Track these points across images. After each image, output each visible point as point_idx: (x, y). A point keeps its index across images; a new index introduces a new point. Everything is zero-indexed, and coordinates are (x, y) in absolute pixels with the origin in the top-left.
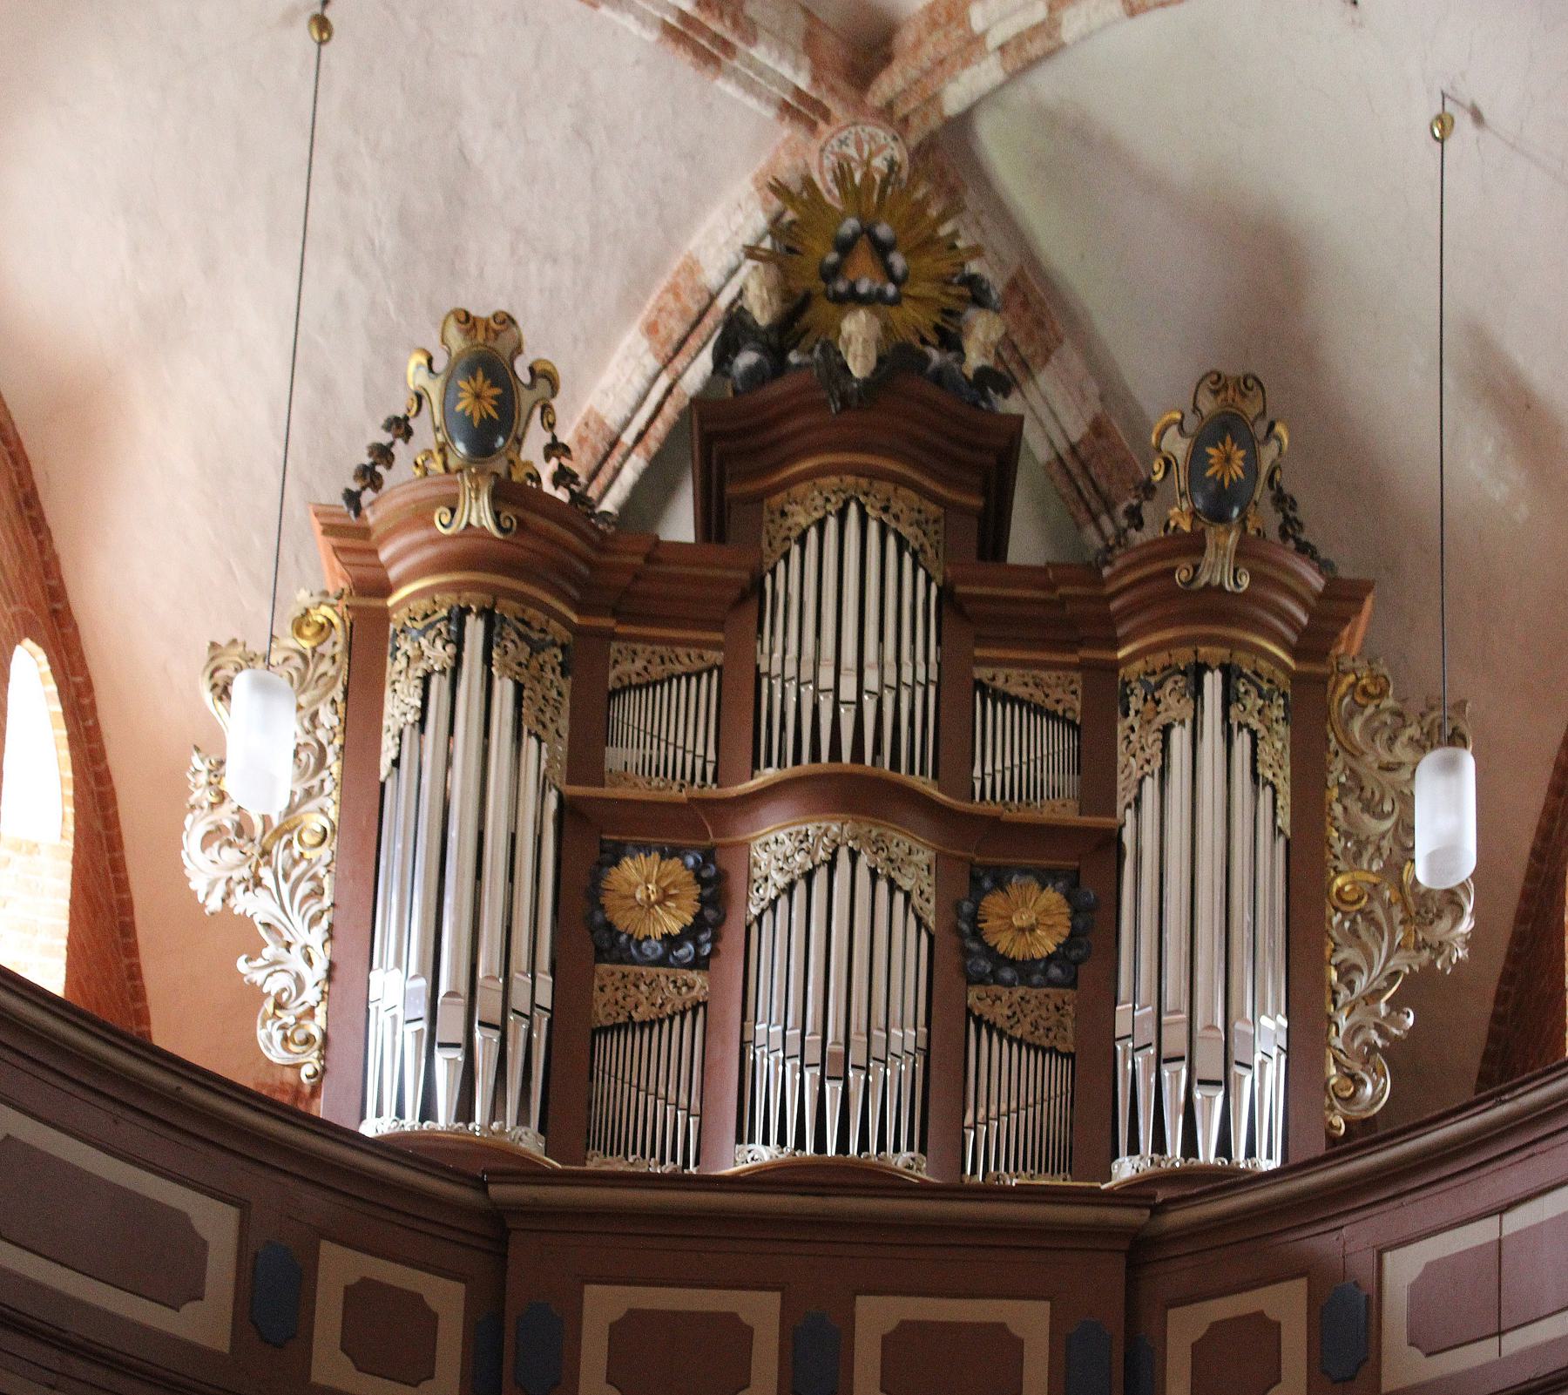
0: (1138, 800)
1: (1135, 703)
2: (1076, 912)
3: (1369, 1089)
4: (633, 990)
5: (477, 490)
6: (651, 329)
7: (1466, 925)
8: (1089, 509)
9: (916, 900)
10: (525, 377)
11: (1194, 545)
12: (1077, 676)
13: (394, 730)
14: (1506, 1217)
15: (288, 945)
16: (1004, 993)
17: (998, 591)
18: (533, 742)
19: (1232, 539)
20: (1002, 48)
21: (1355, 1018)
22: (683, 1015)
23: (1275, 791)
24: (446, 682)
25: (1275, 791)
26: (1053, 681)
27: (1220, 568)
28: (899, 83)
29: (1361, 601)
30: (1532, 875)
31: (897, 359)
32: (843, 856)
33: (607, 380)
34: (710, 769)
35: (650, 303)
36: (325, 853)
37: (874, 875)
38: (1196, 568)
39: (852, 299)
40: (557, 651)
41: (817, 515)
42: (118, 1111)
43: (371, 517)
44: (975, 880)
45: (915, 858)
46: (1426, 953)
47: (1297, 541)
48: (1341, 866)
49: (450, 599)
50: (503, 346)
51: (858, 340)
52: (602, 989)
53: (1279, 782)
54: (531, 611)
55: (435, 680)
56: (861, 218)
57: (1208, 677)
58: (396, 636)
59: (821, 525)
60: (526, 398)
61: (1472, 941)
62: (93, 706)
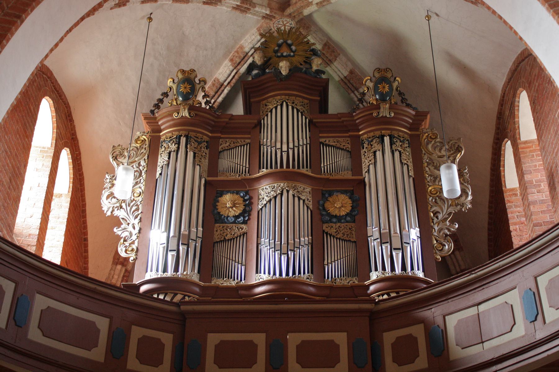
0: (369, 170)
1: (365, 145)
2: (353, 201)
3: (447, 247)
4: (226, 231)
5: (185, 109)
6: (231, 60)
7: (470, 198)
8: (351, 89)
9: (306, 202)
10: (197, 82)
11: (378, 107)
12: (349, 139)
13: (161, 166)
14: (479, 307)
15: (128, 224)
16: (334, 225)
17: (325, 120)
18: (198, 167)
19: (387, 106)
20: (317, 4)
21: (439, 227)
22: (240, 236)
23: (408, 166)
24: (175, 153)
25: (408, 166)
26: (342, 141)
27: (385, 111)
28: (292, 11)
29: (427, 116)
30: (492, 175)
31: (293, 70)
32: (285, 192)
33: (221, 70)
34: (247, 169)
35: (231, 54)
36: (140, 199)
37: (294, 196)
38: (378, 113)
39: (282, 57)
40: (205, 143)
41: (275, 106)
42: (78, 295)
43: (157, 115)
44: (323, 195)
45: (305, 190)
46: (459, 207)
47: (406, 103)
48: (430, 184)
49: (177, 133)
50: (192, 76)
51: (284, 67)
52: (217, 231)
53: (409, 163)
54: (198, 134)
55: (172, 153)
56: (283, 39)
57: (385, 138)
58: (162, 142)
59: (276, 108)
60: (198, 87)
61: (472, 202)
62: (80, 158)
